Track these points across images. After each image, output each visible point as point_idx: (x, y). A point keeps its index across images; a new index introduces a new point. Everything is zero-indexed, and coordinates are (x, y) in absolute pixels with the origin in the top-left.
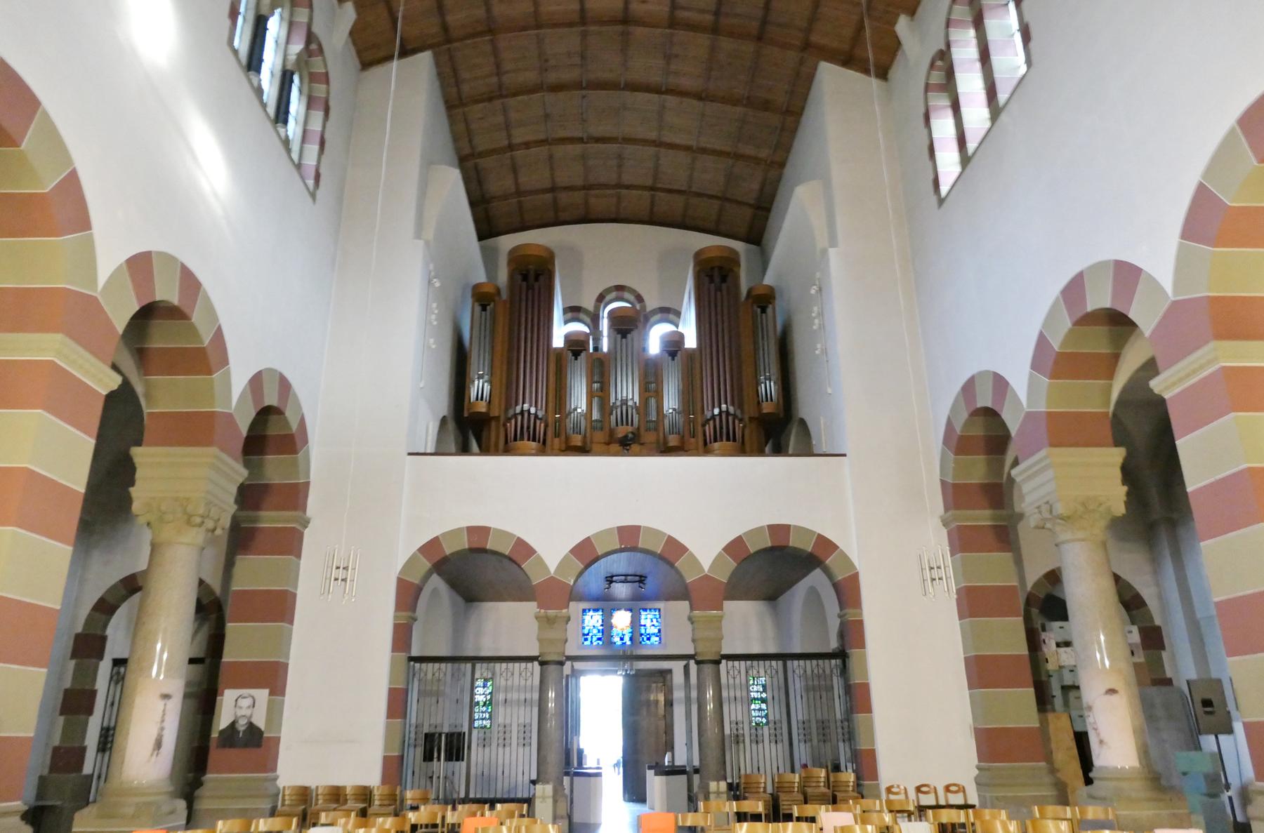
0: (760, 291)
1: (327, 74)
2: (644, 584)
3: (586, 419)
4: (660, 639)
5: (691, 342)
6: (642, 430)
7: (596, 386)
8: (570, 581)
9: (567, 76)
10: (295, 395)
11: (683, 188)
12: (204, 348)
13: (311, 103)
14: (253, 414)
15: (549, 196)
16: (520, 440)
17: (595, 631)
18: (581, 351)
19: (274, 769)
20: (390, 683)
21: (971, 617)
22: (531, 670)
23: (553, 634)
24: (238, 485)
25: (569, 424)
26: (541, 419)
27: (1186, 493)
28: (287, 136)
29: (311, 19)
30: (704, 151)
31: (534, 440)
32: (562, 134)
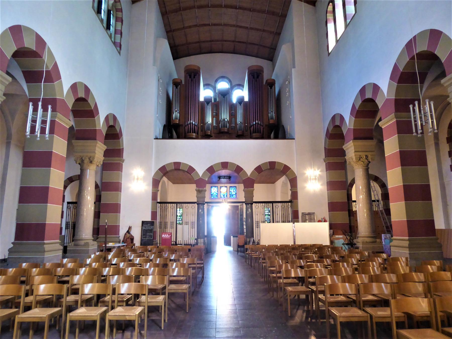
3: (211, 126)
5: (246, 99)
6: (230, 129)
7: (214, 114)
10: (118, 121)
11: (245, 41)
12: (50, 70)
13: (117, 20)
14: (74, 100)
15: (198, 44)
17: (215, 194)
19: (119, 234)
20: (152, 210)
23: (200, 195)
25: (206, 126)
26: (196, 126)
28: (102, 18)
30: (252, 29)
31: (194, 133)
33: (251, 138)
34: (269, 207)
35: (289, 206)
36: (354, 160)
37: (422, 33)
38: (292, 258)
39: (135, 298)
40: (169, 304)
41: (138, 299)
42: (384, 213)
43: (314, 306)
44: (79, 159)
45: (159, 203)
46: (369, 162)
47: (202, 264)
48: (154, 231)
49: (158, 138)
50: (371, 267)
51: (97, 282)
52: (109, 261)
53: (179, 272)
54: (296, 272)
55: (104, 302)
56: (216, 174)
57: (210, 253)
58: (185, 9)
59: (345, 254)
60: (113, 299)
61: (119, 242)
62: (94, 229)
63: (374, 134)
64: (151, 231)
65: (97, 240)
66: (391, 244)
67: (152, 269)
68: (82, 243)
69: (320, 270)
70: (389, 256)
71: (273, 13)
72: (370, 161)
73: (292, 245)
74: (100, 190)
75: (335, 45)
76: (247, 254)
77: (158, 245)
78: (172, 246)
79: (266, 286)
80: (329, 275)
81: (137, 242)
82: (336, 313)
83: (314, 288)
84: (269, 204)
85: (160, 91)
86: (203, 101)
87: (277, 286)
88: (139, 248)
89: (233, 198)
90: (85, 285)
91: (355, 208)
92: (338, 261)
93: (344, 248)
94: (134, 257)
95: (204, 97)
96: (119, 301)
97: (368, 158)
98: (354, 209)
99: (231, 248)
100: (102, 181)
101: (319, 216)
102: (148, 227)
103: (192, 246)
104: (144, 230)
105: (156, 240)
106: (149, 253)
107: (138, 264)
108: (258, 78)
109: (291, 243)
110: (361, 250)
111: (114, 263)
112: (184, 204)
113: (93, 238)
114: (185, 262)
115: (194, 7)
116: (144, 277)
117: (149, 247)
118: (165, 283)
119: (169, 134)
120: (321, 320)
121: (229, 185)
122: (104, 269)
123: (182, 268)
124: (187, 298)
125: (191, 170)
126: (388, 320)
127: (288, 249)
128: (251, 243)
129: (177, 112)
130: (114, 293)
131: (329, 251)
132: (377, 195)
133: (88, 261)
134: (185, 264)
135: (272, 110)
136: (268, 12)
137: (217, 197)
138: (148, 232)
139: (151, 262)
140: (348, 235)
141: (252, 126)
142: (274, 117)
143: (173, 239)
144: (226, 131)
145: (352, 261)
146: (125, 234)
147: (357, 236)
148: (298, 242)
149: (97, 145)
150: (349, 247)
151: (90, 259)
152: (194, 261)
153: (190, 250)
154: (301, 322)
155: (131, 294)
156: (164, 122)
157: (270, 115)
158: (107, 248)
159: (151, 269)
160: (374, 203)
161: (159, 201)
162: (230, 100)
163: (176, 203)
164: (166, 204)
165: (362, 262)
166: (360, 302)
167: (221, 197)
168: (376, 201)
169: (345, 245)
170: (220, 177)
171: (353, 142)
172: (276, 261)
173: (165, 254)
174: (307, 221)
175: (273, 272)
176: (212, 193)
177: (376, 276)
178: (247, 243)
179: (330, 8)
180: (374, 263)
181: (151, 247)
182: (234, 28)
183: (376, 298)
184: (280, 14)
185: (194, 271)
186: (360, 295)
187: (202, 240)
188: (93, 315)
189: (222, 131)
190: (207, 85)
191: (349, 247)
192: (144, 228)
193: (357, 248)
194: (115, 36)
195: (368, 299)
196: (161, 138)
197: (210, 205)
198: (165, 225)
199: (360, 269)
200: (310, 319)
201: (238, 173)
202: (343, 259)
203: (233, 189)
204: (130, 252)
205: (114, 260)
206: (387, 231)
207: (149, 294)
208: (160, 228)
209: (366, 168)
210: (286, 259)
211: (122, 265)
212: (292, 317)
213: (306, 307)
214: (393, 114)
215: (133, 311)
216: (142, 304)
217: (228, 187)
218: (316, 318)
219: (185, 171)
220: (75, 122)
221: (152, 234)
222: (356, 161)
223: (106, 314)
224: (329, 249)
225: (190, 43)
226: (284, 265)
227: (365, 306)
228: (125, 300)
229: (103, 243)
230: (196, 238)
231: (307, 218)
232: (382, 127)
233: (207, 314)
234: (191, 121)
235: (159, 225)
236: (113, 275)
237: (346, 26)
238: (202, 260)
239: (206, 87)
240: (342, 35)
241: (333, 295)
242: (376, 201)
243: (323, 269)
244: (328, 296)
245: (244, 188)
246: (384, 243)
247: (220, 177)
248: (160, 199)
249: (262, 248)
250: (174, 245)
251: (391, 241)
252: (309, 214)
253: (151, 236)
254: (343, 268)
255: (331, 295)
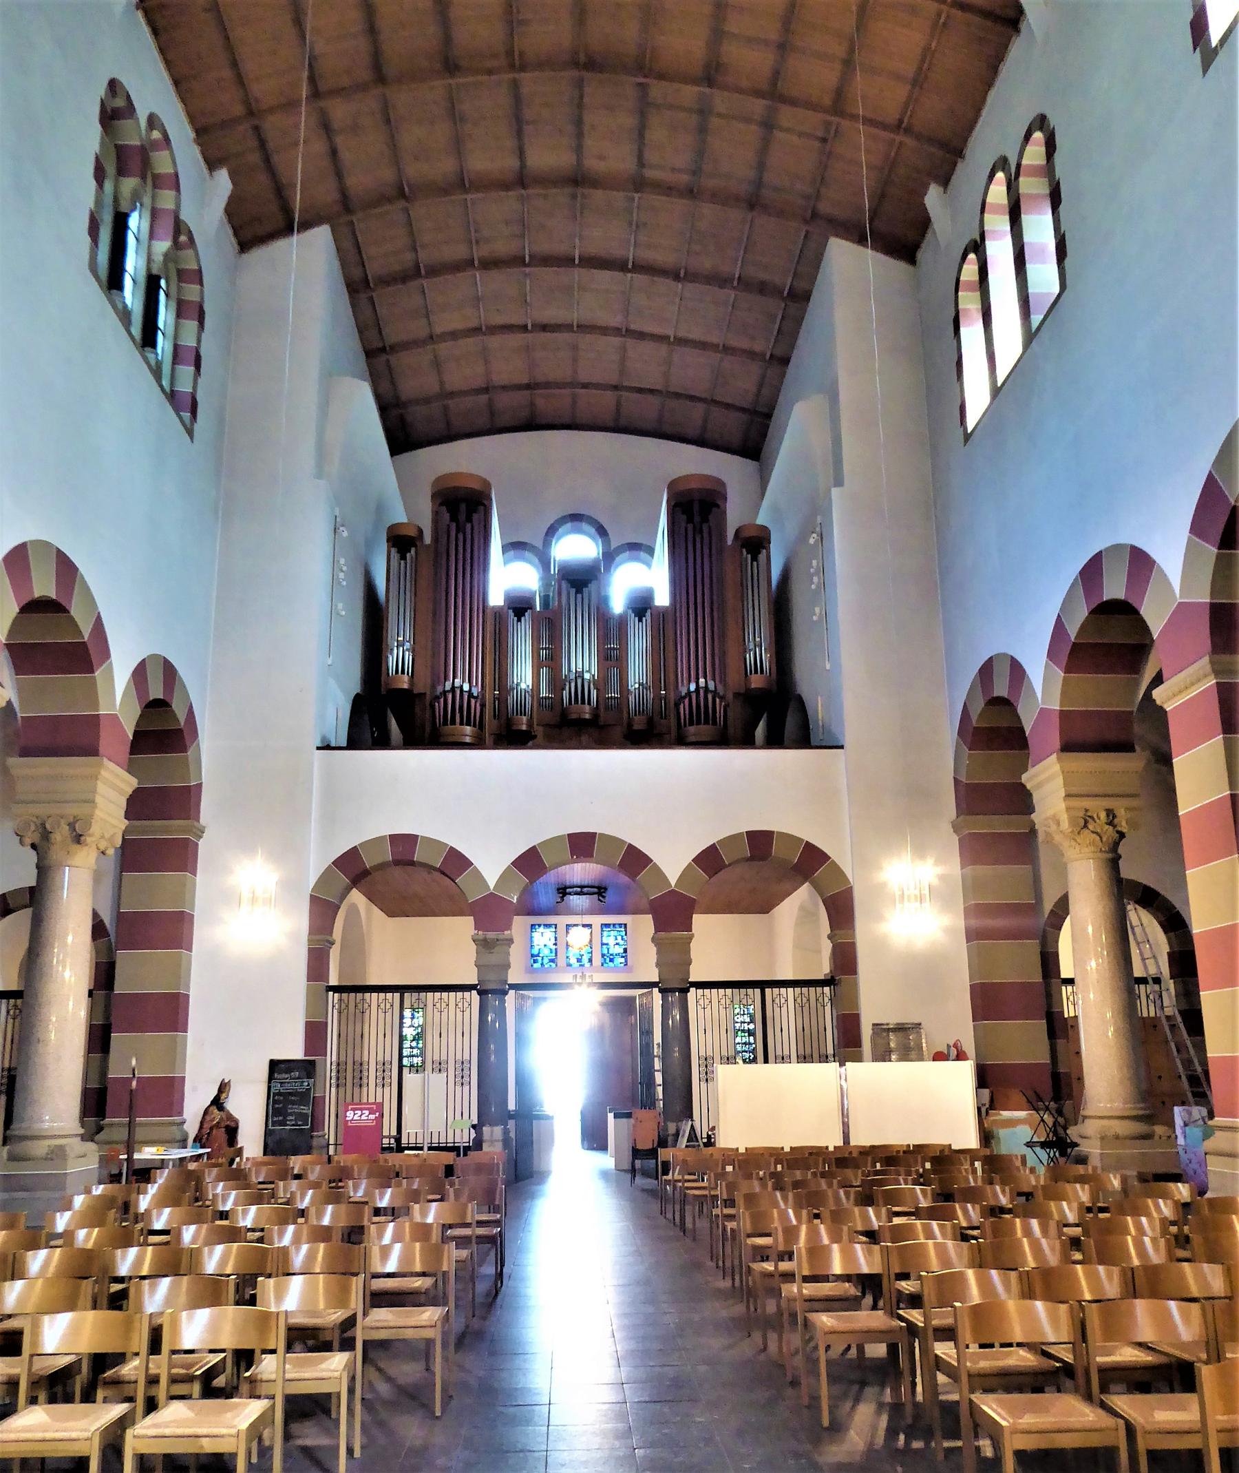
0: (752, 533)
1: (200, 271)
2: (604, 897)
4: (626, 961)
5: (662, 598)
8: (513, 898)
9: (502, 248)
13: (182, 310)
14: (16, 609)
15: (483, 398)
16: (451, 724)
18: (525, 610)
19: (180, 1113)
21: (977, 939)
22: (468, 1000)
23: (493, 959)
24: (128, 797)
26: (476, 698)
27: (1178, 817)
28: (125, 306)
29: (178, 205)
30: (682, 342)
31: (468, 724)
32: (499, 320)
33: (681, 741)
34: (750, 1002)
35: (826, 1000)
36: (1065, 825)
37: (1117, 548)
38: (837, 1198)
39: (237, 1364)
40: (369, 1385)
41: (247, 1371)
42: (1182, 1026)
43: (919, 1388)
44: (33, 828)
45: (335, 989)
46: (1122, 835)
47: (497, 1223)
48: (314, 1097)
49: (333, 744)
50: (1129, 1238)
51: (95, 1307)
52: (142, 1221)
53: (406, 1257)
54: (848, 1256)
55: (117, 1382)
56: (551, 878)
57: (527, 1178)
58: (435, 271)
59: (1034, 1183)
60: (153, 1370)
61: (183, 1144)
62: (86, 1093)
63: (1138, 729)
64: (304, 1097)
65: (98, 1137)
66: (1209, 1144)
67: (305, 1248)
68: (40, 1148)
69: (941, 1249)
70: (1202, 1193)
71: (762, 288)
72: (1124, 831)
73: (835, 1147)
74: (110, 940)
75: (991, 403)
76: (668, 1182)
77: (331, 1152)
78: (382, 1157)
79: (739, 1309)
80: (971, 1266)
81: (251, 1141)
82: (999, 1414)
83: (915, 1316)
84: (750, 991)
85: (342, 571)
86: (501, 608)
87: (780, 1312)
88: (258, 1164)
89: (615, 969)
90: (46, 1318)
91: (1071, 1007)
92: (1009, 1211)
93: (1031, 1160)
94: (236, 1204)
95: (505, 592)
96: (174, 1380)
97: (1116, 821)
98: (1069, 1012)
99: (607, 1161)
100: (119, 908)
101: (936, 1036)
102: (291, 1083)
103: (458, 1155)
104: (280, 1094)
105: (320, 1134)
106: (294, 1185)
107: (253, 1230)
108: (707, 521)
109: (832, 1140)
110: (1095, 1169)
111: (158, 1226)
112: (430, 995)
113: (82, 1131)
114: (430, 1220)
115: (469, 263)
116: (272, 1281)
117: (296, 1163)
118: (353, 1305)
119: (372, 729)
120: (946, 1444)
121: (597, 920)
122: (119, 1252)
123: (418, 1245)
124: (438, 1359)
125: (456, 862)
126: (1193, 1443)
127: (821, 1161)
128: (683, 1142)
129: (403, 646)
130: (155, 1346)
131: (974, 1171)
132: (1154, 957)
133: (62, 1222)
134: (430, 1225)
135: (758, 639)
136: (745, 284)
137: (553, 965)
138: (293, 1103)
139: (301, 1220)
140: (1047, 1109)
141: (684, 697)
142: (766, 665)
143: (389, 1128)
144: (587, 716)
145: (1061, 1212)
146: (206, 1112)
147: (1082, 1113)
148: (862, 1138)
149: (104, 773)
150: (1052, 1155)
151: (68, 1214)
152: (464, 1214)
153: (449, 1170)
154: (870, 1450)
155: (223, 1351)
156: (354, 683)
157: (750, 657)
158: (136, 1167)
159: (298, 1250)
160: (1142, 987)
161: (333, 981)
162: (604, 601)
163: (401, 989)
164: (359, 995)
165: (1101, 1215)
166: (1087, 1372)
167: (569, 965)
168: (1150, 981)
169: (1038, 1149)
170: (566, 888)
171: (1058, 759)
172: (775, 1211)
173: (356, 1189)
174: (893, 1057)
175: (762, 1254)
176: (535, 951)
177: (1152, 1271)
178: (666, 1141)
179: (970, 271)
180: (1144, 1219)
181: (303, 1161)
182: (616, 341)
183: (1150, 1358)
184: (786, 292)
185: (464, 1253)
186: (1087, 1346)
187: (498, 1130)
188: (74, 1435)
189: (574, 716)
190: (515, 547)
191: (1052, 1155)
192: (276, 1087)
193: (1082, 1160)
194: (173, 370)
195: (1117, 1362)
196: (345, 745)
197: (529, 997)
198: (357, 1074)
199: (1090, 1244)
200: (902, 1437)
201: (633, 875)
202: (1028, 1202)
203: (615, 933)
204: (221, 1184)
205: (159, 1215)
206: (1195, 1095)
207: (289, 1348)
208: (338, 1086)
209: (1110, 856)
210: (812, 1204)
211: (188, 1234)
212: (837, 1428)
213: (889, 1390)
214: (1206, 659)
215: (229, 1415)
216: (263, 1389)
217: (597, 928)
218: (928, 1435)
219: (435, 869)
220: (20, 690)
221: (307, 1110)
222: (1072, 832)
223: (124, 1430)
224: (977, 1164)
225: (452, 395)
226: (804, 1228)
227: (1112, 1387)
228: (198, 1373)
229: (121, 1147)
230: (475, 1122)
231: (892, 1045)
232: (1165, 706)
233: (514, 1421)
234: (458, 682)
235: (334, 1074)
236: (154, 1276)
237: (1030, 337)
238: (496, 1209)
239: (512, 553)
240: (1015, 366)
241: (992, 1346)
242: (1150, 981)
243: (950, 1244)
244: (974, 1348)
245: (656, 932)
246: (1181, 1141)
247: (563, 891)
248: (340, 977)
249: (723, 1160)
250: (390, 1149)
251: (1208, 1134)
252: (901, 1029)
253: (303, 1117)
254: (1025, 1240)
255: (982, 1346)
